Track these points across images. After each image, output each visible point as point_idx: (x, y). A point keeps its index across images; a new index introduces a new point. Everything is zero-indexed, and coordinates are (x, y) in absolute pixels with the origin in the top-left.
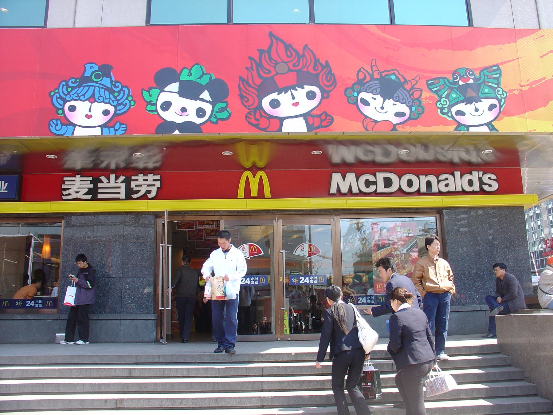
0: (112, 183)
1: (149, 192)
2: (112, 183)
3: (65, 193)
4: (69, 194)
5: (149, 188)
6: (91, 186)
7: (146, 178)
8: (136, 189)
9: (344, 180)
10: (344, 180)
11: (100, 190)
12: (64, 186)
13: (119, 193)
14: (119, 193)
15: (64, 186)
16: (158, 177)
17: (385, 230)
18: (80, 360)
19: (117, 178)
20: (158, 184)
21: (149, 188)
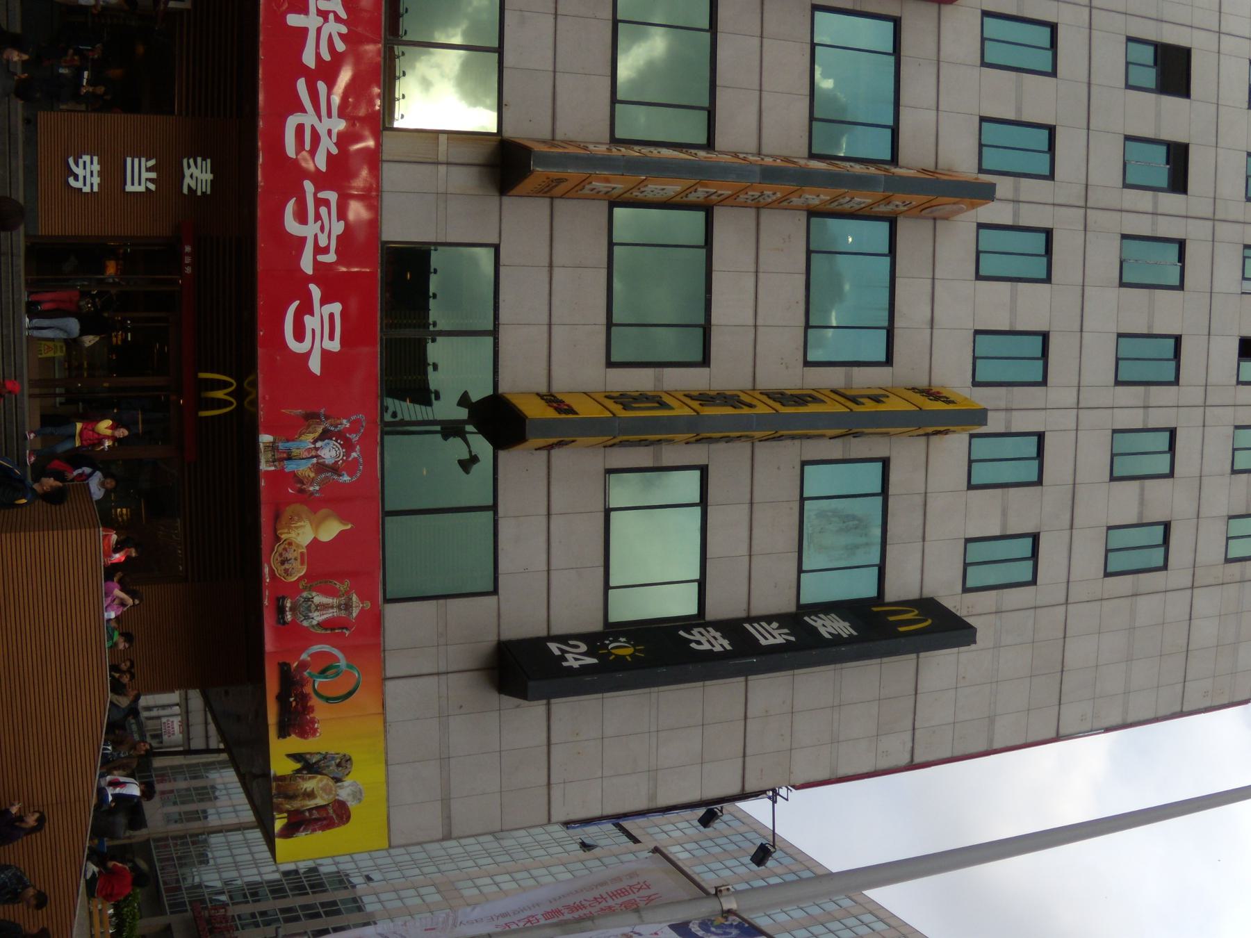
0: (145, 175)
1: (76, 178)
2: (145, 175)
3: (191, 161)
4: (189, 167)
5: (81, 178)
6: (199, 193)
7: (95, 174)
8: (81, 162)
9: (289, 756)
10: (289, 756)
11: (136, 161)
12: (199, 160)
13: (133, 184)
14: (133, 184)
15: (199, 160)
16: (96, 189)
17: (134, 790)
18: (698, 869)
19: (151, 180)
20: (87, 189)
21: (81, 178)
